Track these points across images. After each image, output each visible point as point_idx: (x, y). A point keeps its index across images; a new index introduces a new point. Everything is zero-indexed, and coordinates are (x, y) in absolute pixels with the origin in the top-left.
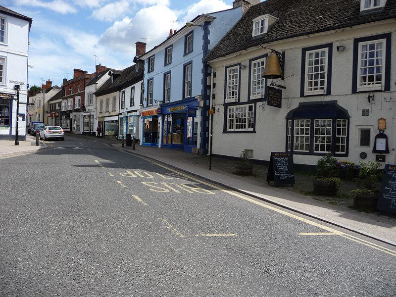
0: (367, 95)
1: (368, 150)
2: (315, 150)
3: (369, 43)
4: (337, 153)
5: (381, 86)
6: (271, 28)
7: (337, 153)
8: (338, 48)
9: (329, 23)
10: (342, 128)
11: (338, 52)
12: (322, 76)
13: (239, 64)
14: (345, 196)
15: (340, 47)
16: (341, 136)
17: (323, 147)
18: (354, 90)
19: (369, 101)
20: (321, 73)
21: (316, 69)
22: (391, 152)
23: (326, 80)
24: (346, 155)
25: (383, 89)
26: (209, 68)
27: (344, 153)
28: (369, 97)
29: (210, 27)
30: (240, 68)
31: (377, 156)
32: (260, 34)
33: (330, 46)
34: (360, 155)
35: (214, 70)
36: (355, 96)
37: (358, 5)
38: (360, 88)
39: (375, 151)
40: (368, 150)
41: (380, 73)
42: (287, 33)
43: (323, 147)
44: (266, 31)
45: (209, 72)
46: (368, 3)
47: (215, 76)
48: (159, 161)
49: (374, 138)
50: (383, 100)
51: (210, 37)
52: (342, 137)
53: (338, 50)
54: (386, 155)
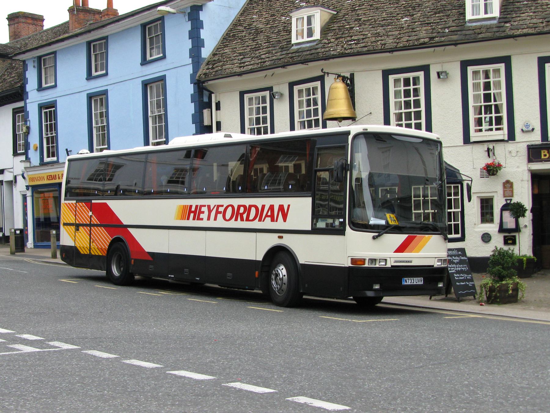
0: (485, 147)
1: (492, 228)
2: (414, 210)
3: (402, 76)
4: (449, 236)
5: (503, 134)
6: (325, 31)
7: (449, 236)
8: (438, 74)
9: (423, 34)
10: (453, 197)
11: (439, 80)
12: (417, 104)
13: (270, 89)
14: (455, 190)
15: (442, 72)
16: (453, 210)
17: (425, 202)
18: (467, 140)
19: (489, 155)
20: (415, 112)
21: (407, 105)
22: (523, 230)
23: (423, 108)
24: (462, 239)
25: (506, 138)
26: (206, 93)
27: (459, 236)
28: (488, 150)
29: (203, 16)
30: (272, 97)
31: (505, 237)
32: (306, 39)
33: (426, 69)
34: (482, 237)
35: (216, 97)
36: (468, 147)
37: (462, 6)
38: (474, 136)
39: (501, 230)
40: (492, 228)
41: (500, 125)
42: (356, 44)
43: (425, 202)
44: (317, 36)
45: (206, 99)
46: (475, 8)
47: (218, 107)
48: (131, 28)
49: (499, 210)
50: (508, 155)
51: (203, 34)
52: (454, 212)
53: (439, 77)
54: (516, 234)
